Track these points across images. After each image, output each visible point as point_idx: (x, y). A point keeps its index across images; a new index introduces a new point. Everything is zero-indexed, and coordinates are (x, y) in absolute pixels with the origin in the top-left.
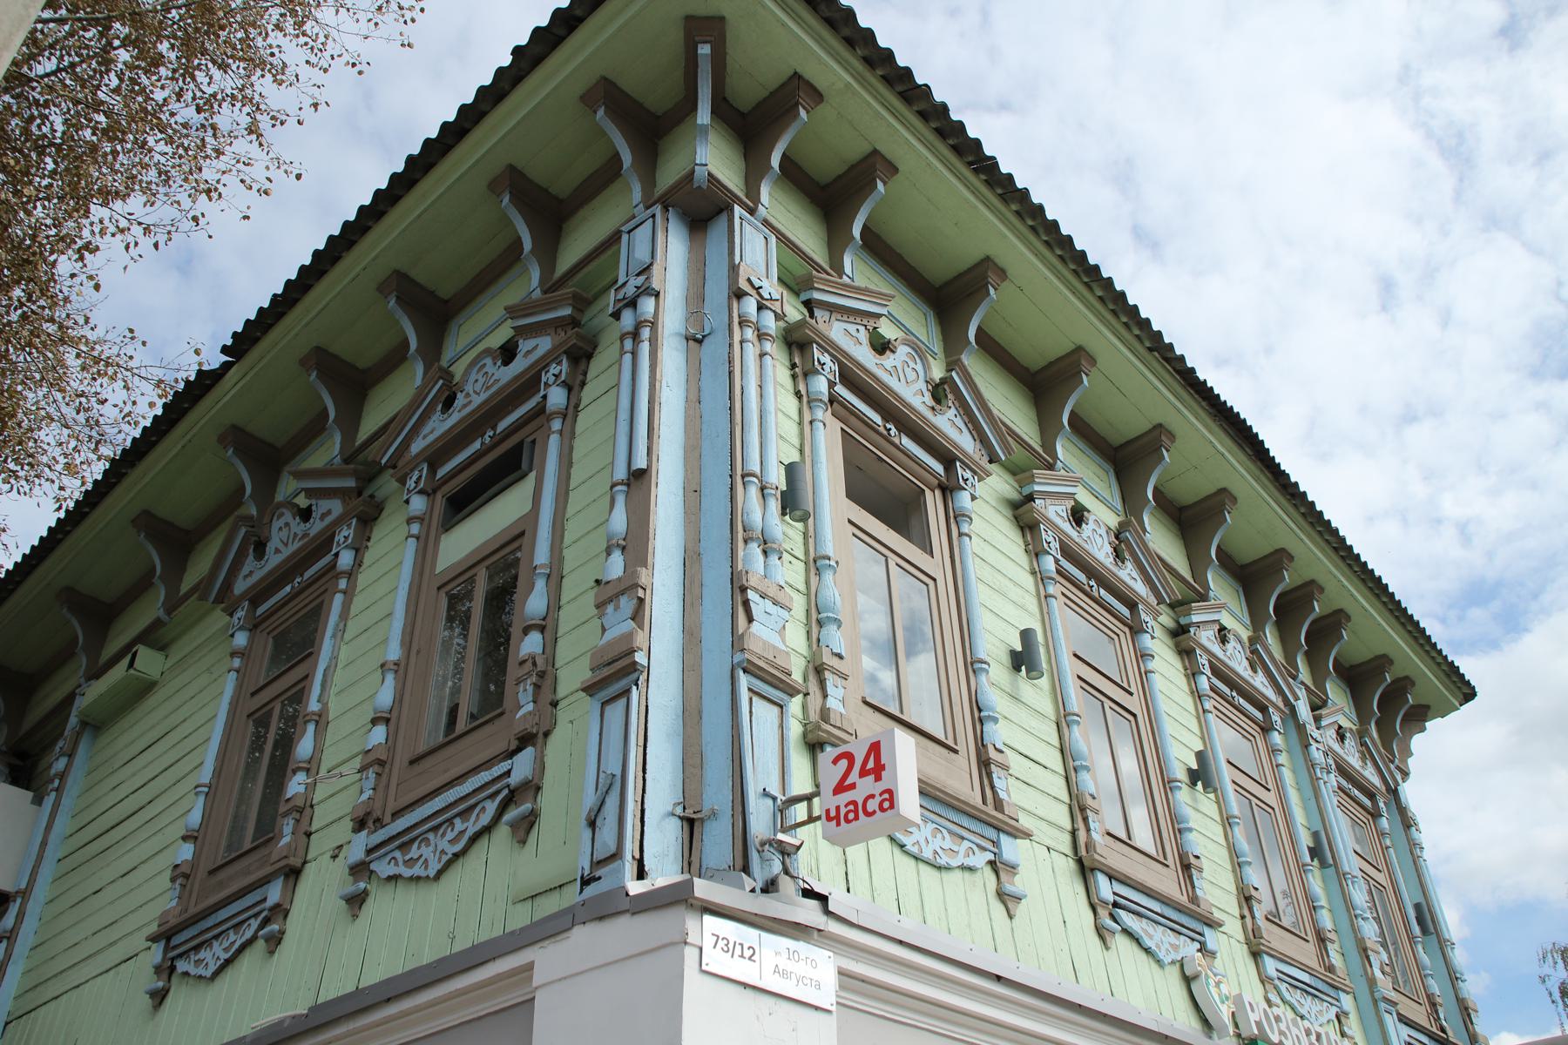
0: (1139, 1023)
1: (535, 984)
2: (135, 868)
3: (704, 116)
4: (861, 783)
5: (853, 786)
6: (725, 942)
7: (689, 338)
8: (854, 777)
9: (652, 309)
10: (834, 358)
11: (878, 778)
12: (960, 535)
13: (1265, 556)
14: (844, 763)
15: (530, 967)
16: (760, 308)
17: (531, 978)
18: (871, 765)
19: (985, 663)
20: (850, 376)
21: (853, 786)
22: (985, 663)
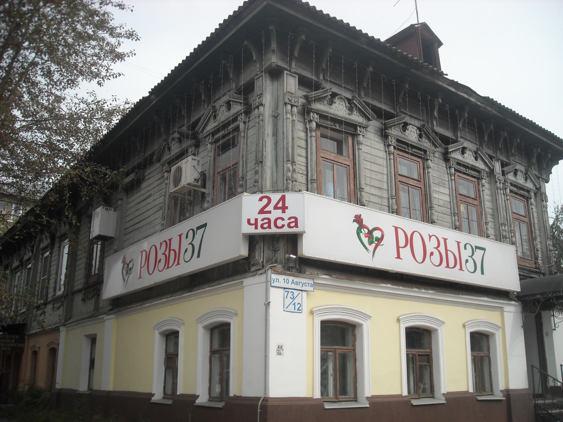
0: (457, 246)
1: (244, 285)
2: (140, 222)
3: (274, 46)
4: (274, 212)
5: (269, 212)
6: (292, 293)
7: (274, 116)
8: (270, 208)
9: (263, 110)
10: (317, 114)
11: (284, 212)
12: (359, 149)
13: (489, 342)
14: (265, 201)
15: (243, 281)
16: (500, 183)
17: (243, 284)
18: (280, 205)
19: (363, 189)
20: (323, 116)
21: (269, 212)
22: (363, 189)
